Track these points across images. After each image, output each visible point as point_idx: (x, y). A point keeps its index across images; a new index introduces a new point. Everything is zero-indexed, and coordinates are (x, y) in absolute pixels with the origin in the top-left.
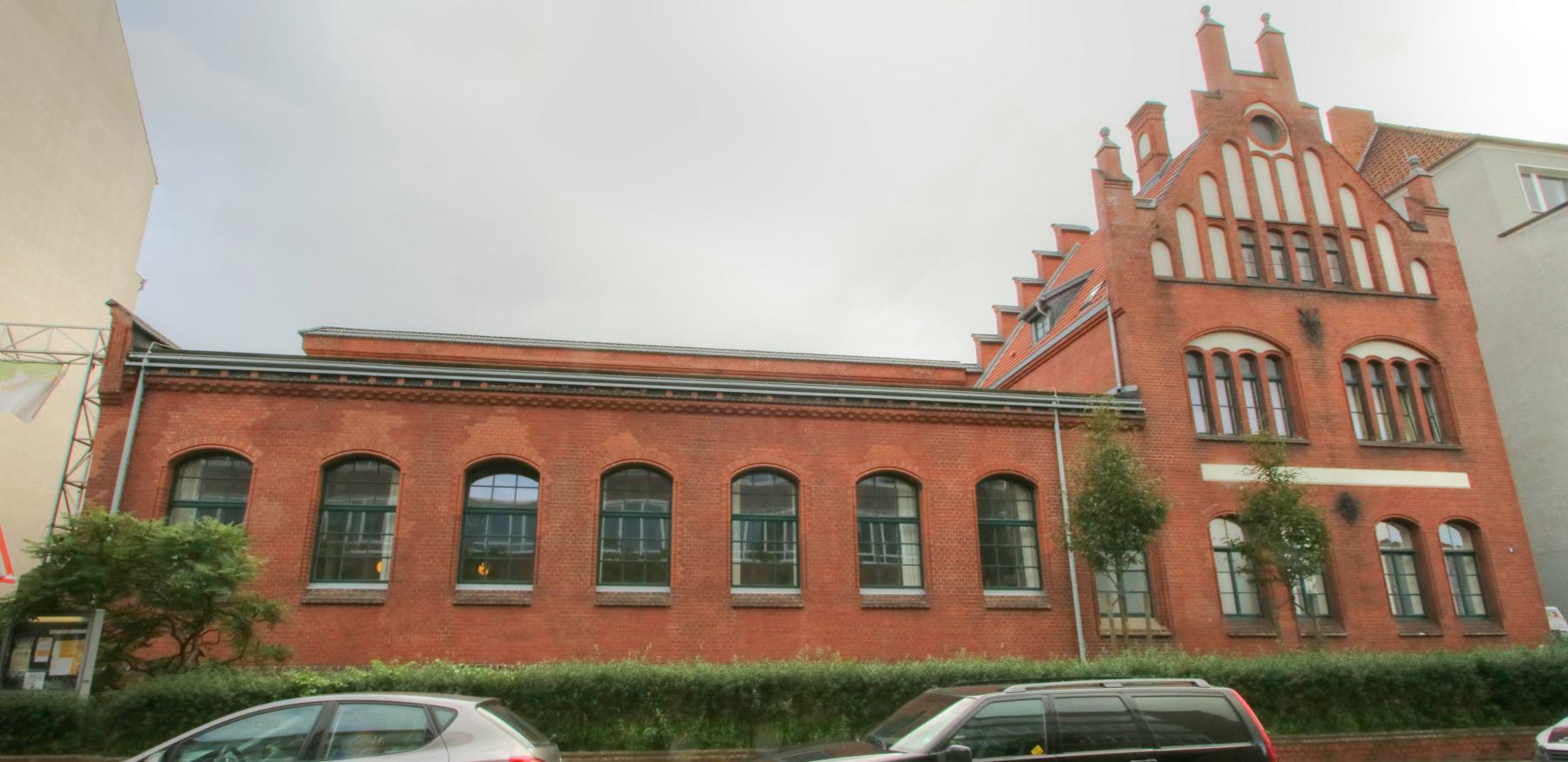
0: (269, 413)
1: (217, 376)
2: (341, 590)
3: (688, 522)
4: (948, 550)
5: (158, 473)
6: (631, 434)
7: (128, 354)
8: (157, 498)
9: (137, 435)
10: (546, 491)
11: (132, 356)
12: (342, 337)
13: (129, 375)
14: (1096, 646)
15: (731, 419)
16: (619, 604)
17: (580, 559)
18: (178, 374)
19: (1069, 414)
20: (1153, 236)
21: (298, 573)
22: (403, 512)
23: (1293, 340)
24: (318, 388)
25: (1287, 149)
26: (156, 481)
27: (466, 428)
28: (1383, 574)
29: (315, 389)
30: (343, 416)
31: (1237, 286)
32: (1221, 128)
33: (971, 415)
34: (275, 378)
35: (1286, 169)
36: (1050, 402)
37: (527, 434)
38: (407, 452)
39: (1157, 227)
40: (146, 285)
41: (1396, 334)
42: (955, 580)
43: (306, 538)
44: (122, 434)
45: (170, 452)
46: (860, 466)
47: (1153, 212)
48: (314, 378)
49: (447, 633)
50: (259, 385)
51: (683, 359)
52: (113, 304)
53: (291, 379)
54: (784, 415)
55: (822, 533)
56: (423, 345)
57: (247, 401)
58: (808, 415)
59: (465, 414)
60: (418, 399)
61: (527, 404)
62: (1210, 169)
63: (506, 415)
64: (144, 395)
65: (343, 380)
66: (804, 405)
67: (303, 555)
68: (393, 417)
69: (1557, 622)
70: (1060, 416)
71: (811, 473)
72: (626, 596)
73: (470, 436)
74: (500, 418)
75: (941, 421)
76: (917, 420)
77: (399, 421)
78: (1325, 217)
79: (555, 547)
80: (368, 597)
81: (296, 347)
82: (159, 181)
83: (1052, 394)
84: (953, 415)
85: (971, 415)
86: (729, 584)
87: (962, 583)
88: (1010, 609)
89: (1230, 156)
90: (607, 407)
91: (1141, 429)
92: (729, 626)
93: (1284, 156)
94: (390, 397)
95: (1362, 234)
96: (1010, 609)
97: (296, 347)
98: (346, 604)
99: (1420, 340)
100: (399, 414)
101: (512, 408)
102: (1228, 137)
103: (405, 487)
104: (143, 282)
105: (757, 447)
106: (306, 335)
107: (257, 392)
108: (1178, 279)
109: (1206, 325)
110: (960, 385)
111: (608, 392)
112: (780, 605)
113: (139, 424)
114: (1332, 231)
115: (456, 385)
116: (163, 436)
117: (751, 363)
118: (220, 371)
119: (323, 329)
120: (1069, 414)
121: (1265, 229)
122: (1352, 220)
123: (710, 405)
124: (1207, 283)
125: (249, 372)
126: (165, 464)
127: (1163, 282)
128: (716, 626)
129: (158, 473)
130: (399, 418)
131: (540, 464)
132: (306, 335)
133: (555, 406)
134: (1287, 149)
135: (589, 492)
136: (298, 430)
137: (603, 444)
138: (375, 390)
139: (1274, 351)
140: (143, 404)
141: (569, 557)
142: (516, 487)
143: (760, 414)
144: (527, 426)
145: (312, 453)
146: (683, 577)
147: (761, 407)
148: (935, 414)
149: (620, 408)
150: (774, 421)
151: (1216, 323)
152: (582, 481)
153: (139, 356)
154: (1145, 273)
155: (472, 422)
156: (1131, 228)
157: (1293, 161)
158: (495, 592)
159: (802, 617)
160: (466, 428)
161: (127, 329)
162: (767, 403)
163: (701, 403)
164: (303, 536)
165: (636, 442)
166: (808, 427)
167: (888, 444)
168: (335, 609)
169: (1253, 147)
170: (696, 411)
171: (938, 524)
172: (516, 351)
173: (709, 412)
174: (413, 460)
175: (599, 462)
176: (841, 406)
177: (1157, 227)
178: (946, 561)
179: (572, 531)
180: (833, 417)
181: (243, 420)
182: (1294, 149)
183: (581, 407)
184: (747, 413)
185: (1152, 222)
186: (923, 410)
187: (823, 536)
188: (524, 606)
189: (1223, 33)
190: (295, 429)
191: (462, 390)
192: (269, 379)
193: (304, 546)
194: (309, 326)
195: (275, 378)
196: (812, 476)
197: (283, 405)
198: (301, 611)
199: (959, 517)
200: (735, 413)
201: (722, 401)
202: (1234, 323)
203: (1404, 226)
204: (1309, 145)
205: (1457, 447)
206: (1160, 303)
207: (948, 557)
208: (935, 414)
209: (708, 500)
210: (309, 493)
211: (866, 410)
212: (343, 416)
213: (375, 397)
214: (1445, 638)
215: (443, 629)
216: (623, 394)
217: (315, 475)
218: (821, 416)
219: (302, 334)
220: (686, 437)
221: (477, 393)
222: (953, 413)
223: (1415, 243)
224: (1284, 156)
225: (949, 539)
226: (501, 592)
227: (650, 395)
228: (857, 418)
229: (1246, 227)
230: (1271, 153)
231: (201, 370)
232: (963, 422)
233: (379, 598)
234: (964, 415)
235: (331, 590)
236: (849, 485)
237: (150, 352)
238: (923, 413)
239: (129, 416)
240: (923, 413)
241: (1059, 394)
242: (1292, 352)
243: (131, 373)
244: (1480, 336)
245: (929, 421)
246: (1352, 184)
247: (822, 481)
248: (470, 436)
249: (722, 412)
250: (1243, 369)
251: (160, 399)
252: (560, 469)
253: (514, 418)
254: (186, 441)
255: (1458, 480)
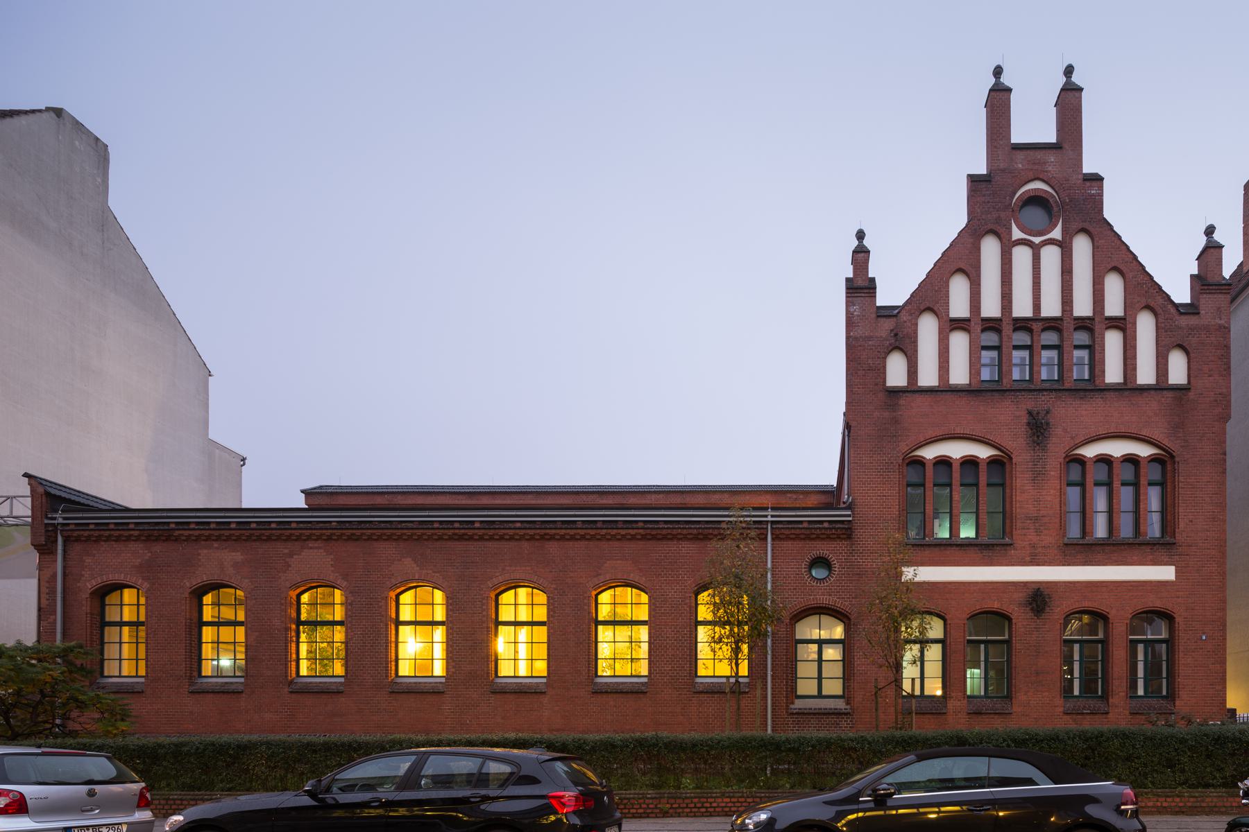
0: (150, 554)
1: (186, 527)
2: (521, 683)
3: (457, 628)
4: (666, 646)
5: (84, 602)
6: (410, 559)
7: (47, 515)
8: (87, 620)
9: (65, 575)
10: (349, 607)
11: (50, 516)
12: (332, 493)
13: (49, 531)
14: (785, 721)
15: (490, 544)
16: (406, 691)
17: (377, 658)
18: (81, 528)
19: (780, 526)
20: (890, 345)
21: (184, 671)
22: (249, 626)
23: (1017, 443)
24: (177, 533)
25: (1056, 234)
26: (84, 608)
27: (287, 560)
28: (147, 660)
29: (74, 535)
30: (199, 554)
31: (972, 391)
32: (984, 217)
33: (690, 531)
34: (146, 527)
35: (1051, 257)
36: (766, 516)
37: (332, 563)
38: (247, 581)
39: (896, 335)
40: (246, 461)
41: (1133, 430)
42: (670, 670)
43: (186, 646)
44: (54, 575)
45: (90, 587)
46: (595, 579)
47: (895, 319)
48: (173, 526)
49: (287, 712)
50: (136, 533)
51: (592, 497)
52: (26, 475)
53: (157, 528)
54: (532, 538)
55: (563, 635)
56: (391, 496)
57: (133, 546)
58: (552, 538)
59: (286, 548)
60: (249, 538)
61: (329, 538)
62: (962, 266)
63: (316, 548)
64: (64, 546)
65: (192, 526)
66: (547, 529)
67: (186, 658)
68: (234, 554)
69: (1233, 699)
70: (772, 528)
71: (554, 586)
72: (414, 685)
73: (290, 566)
74: (311, 551)
75: (664, 538)
76: (644, 538)
77: (238, 556)
78: (1083, 307)
79: (358, 649)
80: (233, 687)
81: (300, 502)
82: (212, 373)
83: (766, 509)
84: (675, 532)
85: (690, 531)
86: (195, 674)
87: (675, 672)
88: (713, 692)
89: (990, 249)
90: (389, 538)
91: (849, 537)
92: (489, 706)
93: (1052, 242)
94: (228, 539)
95: (1123, 325)
96: (713, 692)
97: (300, 502)
98: (218, 692)
99: (1157, 435)
100: (238, 551)
101: (319, 542)
102: (990, 226)
103: (249, 607)
104: (244, 460)
105: (510, 566)
106: (308, 493)
107: (138, 539)
108: (912, 389)
109: (930, 433)
110: (828, 506)
111: (388, 525)
112: (528, 691)
113: (64, 568)
114: (1088, 323)
115: (273, 526)
116: (83, 576)
117: (648, 496)
118: (108, 524)
119: (321, 487)
120: (780, 526)
121: (1011, 327)
122: (1114, 306)
123: (470, 532)
124: (945, 390)
125: (128, 524)
126: (88, 596)
127: (895, 392)
128: (479, 706)
129: (84, 602)
130: (239, 554)
131: (343, 586)
132: (308, 493)
133: (350, 538)
134: (1056, 234)
135: (381, 607)
136: (170, 566)
137: (390, 569)
138: (216, 533)
139: (1155, 454)
140: (65, 551)
141: (369, 657)
142: (433, 604)
143: (512, 538)
144: (332, 557)
145: (182, 584)
146: (453, 670)
147: (511, 532)
148: (659, 531)
149: (399, 538)
150: (525, 544)
151: (940, 432)
152: (376, 598)
153: (54, 516)
154: (876, 384)
155: (291, 555)
156: (870, 338)
157: (1060, 246)
158: (320, 683)
159: (545, 699)
160: (287, 560)
161: (42, 495)
162: (515, 528)
163: (463, 531)
164: (184, 645)
165: (415, 565)
166: (553, 548)
167: (621, 560)
168: (212, 695)
169: (1017, 234)
170: (461, 538)
171: (659, 625)
172: (461, 497)
173: (471, 538)
174: (252, 587)
175: (388, 583)
176: (578, 528)
177: (896, 335)
178: (663, 655)
179: (369, 637)
180: (573, 538)
181: (133, 560)
182: (1064, 231)
183: (370, 538)
184: (502, 538)
185: (892, 330)
186: (648, 528)
187: (564, 637)
188: (339, 692)
189: (1080, 98)
190: (168, 566)
191: (279, 529)
192: (141, 528)
193: (186, 652)
194: (311, 484)
195: (146, 527)
196: (555, 589)
197: (158, 548)
198: (593, 697)
199: (677, 619)
200: (491, 538)
201: (479, 529)
202: (959, 430)
203: (1173, 310)
204: (1081, 225)
205: (1172, 540)
206: (886, 414)
207: (666, 652)
208: (659, 531)
209: (472, 610)
210: (183, 614)
211: (599, 531)
212: (199, 554)
213: (218, 539)
214: (1110, 716)
215: (285, 709)
216: (399, 526)
217: (186, 600)
218: (562, 538)
219: (302, 491)
220: (454, 560)
221: (290, 531)
222: (675, 530)
223: (1180, 328)
224: (1052, 242)
225: (667, 637)
226: (326, 683)
227: (564, 526)
228: (593, 538)
229: (991, 325)
230: (1037, 240)
231: (218, 523)
232: (685, 538)
233: (241, 688)
234: (685, 532)
235: (210, 683)
236: (585, 595)
237: (770, 510)
238: (648, 531)
239: (56, 561)
240: (648, 531)
241: (773, 509)
242: (1013, 456)
243: (50, 529)
244: (1230, 427)
245: (654, 538)
246: (1121, 267)
247: (564, 592)
248: (290, 566)
249: (481, 538)
250: (1127, 473)
251: (77, 548)
252: (359, 590)
253: (322, 551)
254: (99, 578)
255: (1166, 573)
